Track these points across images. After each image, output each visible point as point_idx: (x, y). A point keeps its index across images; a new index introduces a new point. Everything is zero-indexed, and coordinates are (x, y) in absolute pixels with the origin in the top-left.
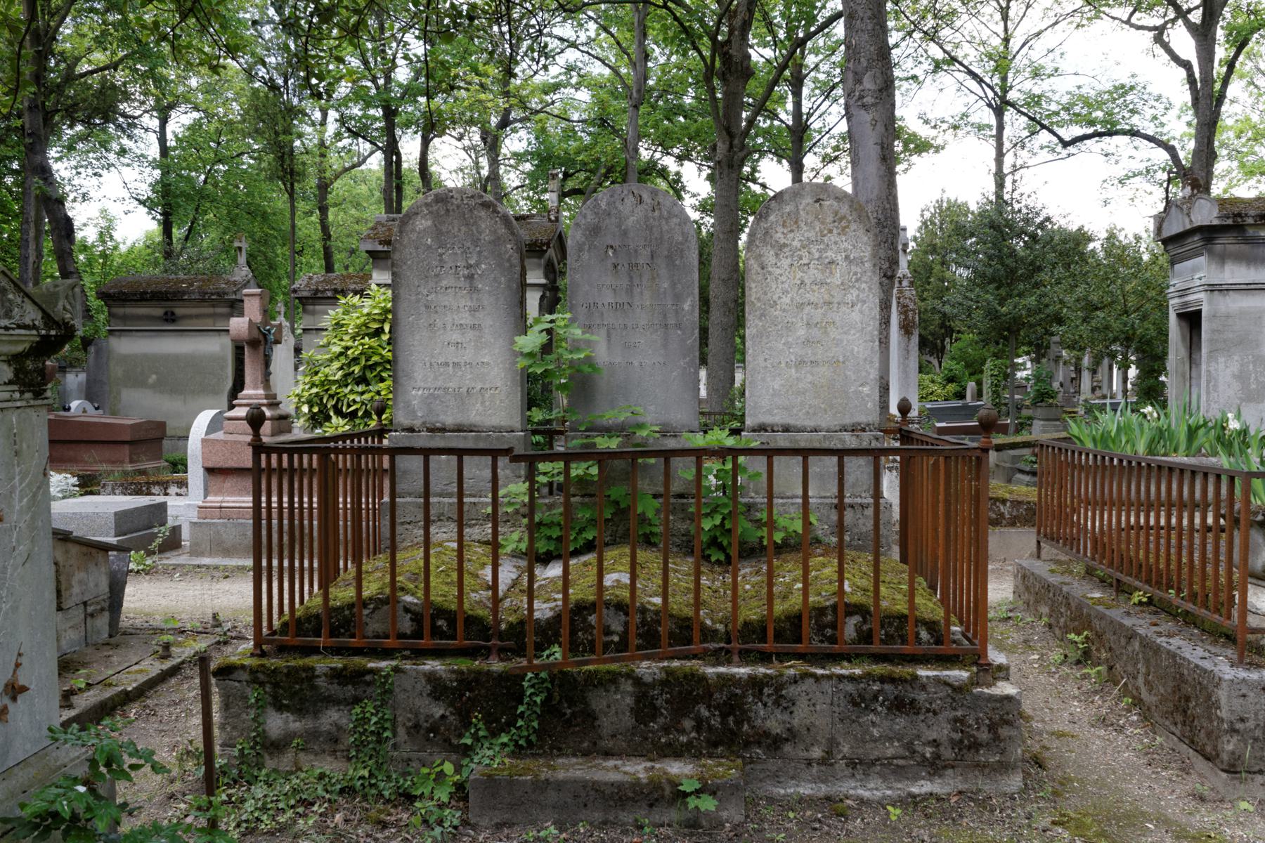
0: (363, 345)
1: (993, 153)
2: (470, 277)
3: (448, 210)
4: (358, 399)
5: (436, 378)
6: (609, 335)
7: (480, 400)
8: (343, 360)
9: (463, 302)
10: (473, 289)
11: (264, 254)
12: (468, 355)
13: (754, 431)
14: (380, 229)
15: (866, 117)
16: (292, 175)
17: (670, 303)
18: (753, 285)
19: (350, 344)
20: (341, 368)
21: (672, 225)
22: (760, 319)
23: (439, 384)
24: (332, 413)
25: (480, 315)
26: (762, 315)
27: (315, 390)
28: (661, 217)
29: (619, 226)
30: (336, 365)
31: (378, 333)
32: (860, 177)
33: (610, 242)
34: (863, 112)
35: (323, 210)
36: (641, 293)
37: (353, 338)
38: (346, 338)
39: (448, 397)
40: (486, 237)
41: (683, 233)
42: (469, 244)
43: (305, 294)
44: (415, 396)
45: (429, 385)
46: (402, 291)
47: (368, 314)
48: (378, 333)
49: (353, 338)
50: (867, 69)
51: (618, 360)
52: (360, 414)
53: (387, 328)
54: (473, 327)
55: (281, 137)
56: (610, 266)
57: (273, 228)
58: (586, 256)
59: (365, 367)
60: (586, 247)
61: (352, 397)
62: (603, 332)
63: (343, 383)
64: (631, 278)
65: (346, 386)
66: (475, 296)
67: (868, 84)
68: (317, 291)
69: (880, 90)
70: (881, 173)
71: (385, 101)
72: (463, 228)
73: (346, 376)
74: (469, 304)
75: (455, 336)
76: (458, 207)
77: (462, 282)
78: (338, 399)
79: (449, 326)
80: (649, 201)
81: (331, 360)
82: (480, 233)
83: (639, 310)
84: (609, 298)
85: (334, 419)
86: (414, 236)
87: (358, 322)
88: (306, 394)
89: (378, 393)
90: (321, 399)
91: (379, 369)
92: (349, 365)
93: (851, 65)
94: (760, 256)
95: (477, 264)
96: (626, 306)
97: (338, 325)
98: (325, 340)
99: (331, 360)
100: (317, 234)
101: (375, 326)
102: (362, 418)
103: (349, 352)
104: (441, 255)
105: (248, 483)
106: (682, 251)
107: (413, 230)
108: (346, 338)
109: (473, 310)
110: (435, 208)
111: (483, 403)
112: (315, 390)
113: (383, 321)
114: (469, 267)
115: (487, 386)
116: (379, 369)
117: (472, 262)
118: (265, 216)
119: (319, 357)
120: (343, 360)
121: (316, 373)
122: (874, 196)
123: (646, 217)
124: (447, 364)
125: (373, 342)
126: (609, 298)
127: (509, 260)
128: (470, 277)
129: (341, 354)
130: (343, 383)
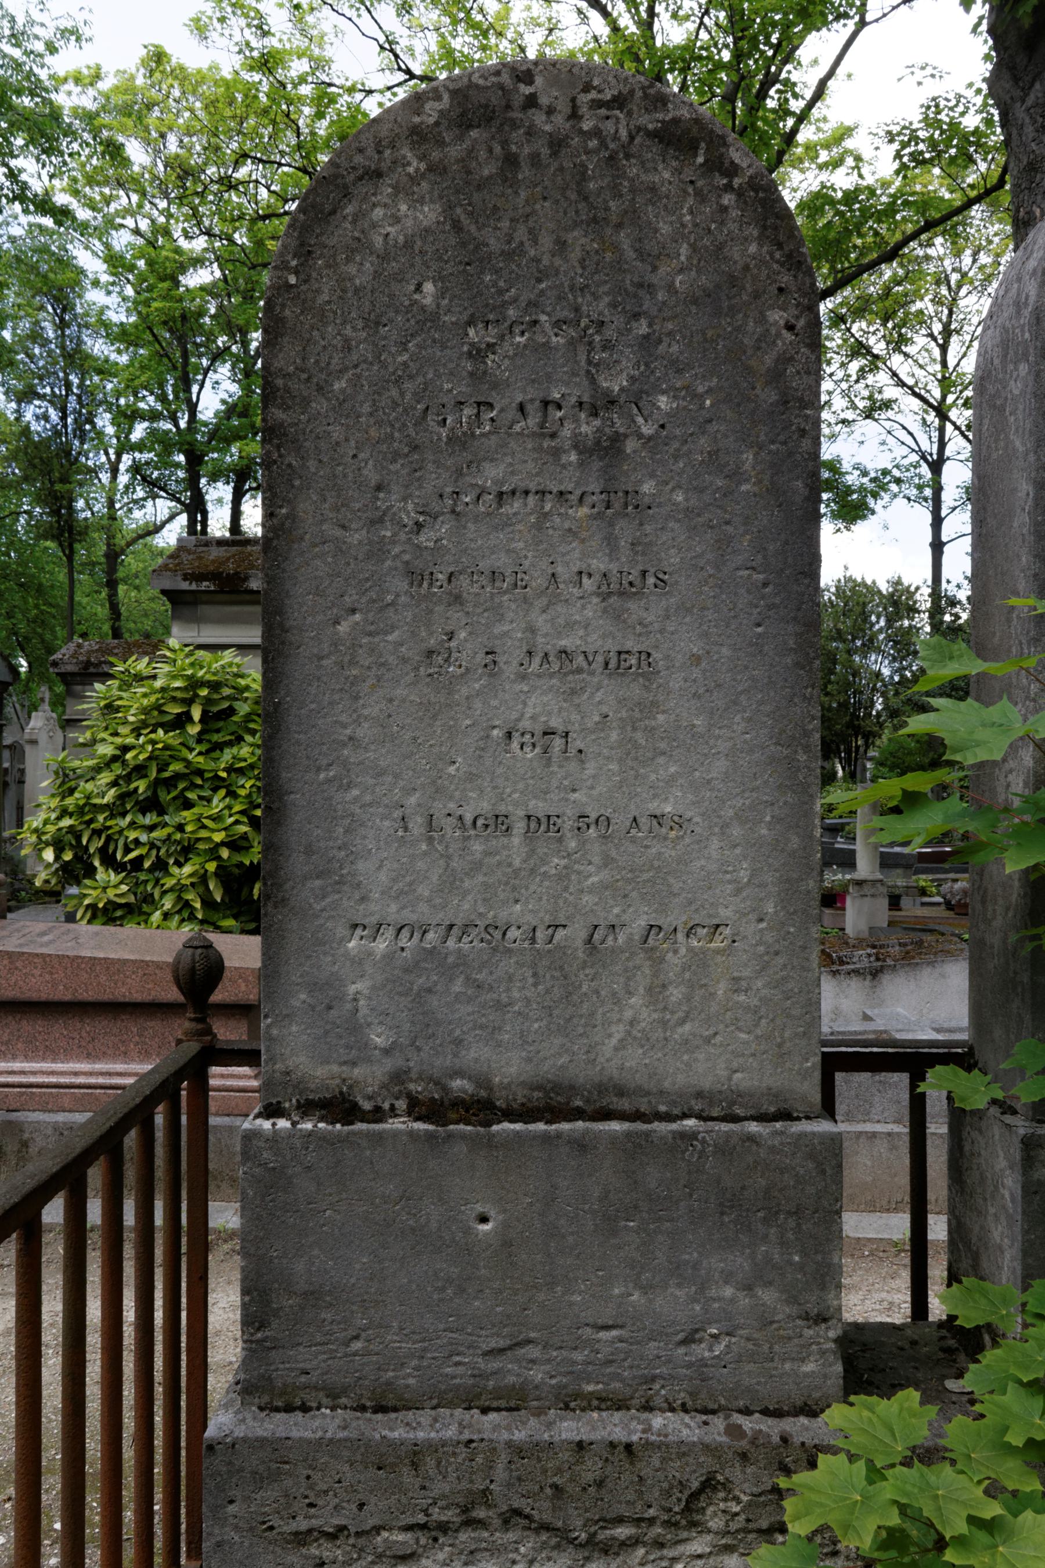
0: (153, 742)
1: (928, 518)
2: (607, 449)
3: (511, 161)
4: (144, 838)
5: (450, 883)
7: (642, 981)
8: (118, 769)
9: (572, 558)
10: (618, 502)
11: (41, 636)
12: (592, 785)
14: (185, 557)
16: (70, 532)
19: (130, 740)
20: (115, 784)
23: (462, 909)
24: (97, 863)
25: (647, 610)
27: (66, 822)
30: (105, 778)
31: (181, 721)
35: (112, 584)
37: (137, 732)
38: (124, 730)
39: (506, 965)
40: (678, 275)
42: (602, 307)
43: (70, 668)
44: (358, 962)
45: (422, 912)
46: (305, 507)
47: (163, 690)
48: (181, 721)
49: (137, 732)
52: (147, 864)
53: (196, 713)
54: (617, 664)
55: (58, 487)
57: (51, 605)
59: (157, 783)
61: (132, 835)
63: (116, 810)
65: (123, 815)
66: (625, 531)
68: (88, 664)
71: (189, 443)
72: (579, 240)
73: (122, 797)
74: (598, 564)
75: (540, 704)
76: (557, 144)
77: (569, 473)
78: (109, 838)
79: (509, 663)
81: (98, 770)
82: (652, 259)
85: (101, 875)
86: (361, 272)
87: (145, 702)
88: (51, 829)
89: (180, 828)
90: (78, 837)
91: (181, 786)
92: (128, 778)
95: (638, 397)
97: (110, 708)
98: (88, 735)
99: (98, 770)
100: (102, 611)
101: (176, 710)
102: (151, 870)
103: (129, 756)
104: (478, 354)
105: (259, 652)
107: (360, 245)
108: (124, 730)
109: (617, 592)
110: (455, 151)
111: (656, 992)
112: (66, 822)
113: (189, 702)
114: (600, 404)
115: (675, 918)
116: (181, 786)
117: (615, 384)
118: (40, 590)
119: (76, 763)
120: (118, 769)
121: (71, 791)
124: (500, 822)
125: (172, 738)
128: (607, 449)
129: (114, 759)
130: (116, 810)
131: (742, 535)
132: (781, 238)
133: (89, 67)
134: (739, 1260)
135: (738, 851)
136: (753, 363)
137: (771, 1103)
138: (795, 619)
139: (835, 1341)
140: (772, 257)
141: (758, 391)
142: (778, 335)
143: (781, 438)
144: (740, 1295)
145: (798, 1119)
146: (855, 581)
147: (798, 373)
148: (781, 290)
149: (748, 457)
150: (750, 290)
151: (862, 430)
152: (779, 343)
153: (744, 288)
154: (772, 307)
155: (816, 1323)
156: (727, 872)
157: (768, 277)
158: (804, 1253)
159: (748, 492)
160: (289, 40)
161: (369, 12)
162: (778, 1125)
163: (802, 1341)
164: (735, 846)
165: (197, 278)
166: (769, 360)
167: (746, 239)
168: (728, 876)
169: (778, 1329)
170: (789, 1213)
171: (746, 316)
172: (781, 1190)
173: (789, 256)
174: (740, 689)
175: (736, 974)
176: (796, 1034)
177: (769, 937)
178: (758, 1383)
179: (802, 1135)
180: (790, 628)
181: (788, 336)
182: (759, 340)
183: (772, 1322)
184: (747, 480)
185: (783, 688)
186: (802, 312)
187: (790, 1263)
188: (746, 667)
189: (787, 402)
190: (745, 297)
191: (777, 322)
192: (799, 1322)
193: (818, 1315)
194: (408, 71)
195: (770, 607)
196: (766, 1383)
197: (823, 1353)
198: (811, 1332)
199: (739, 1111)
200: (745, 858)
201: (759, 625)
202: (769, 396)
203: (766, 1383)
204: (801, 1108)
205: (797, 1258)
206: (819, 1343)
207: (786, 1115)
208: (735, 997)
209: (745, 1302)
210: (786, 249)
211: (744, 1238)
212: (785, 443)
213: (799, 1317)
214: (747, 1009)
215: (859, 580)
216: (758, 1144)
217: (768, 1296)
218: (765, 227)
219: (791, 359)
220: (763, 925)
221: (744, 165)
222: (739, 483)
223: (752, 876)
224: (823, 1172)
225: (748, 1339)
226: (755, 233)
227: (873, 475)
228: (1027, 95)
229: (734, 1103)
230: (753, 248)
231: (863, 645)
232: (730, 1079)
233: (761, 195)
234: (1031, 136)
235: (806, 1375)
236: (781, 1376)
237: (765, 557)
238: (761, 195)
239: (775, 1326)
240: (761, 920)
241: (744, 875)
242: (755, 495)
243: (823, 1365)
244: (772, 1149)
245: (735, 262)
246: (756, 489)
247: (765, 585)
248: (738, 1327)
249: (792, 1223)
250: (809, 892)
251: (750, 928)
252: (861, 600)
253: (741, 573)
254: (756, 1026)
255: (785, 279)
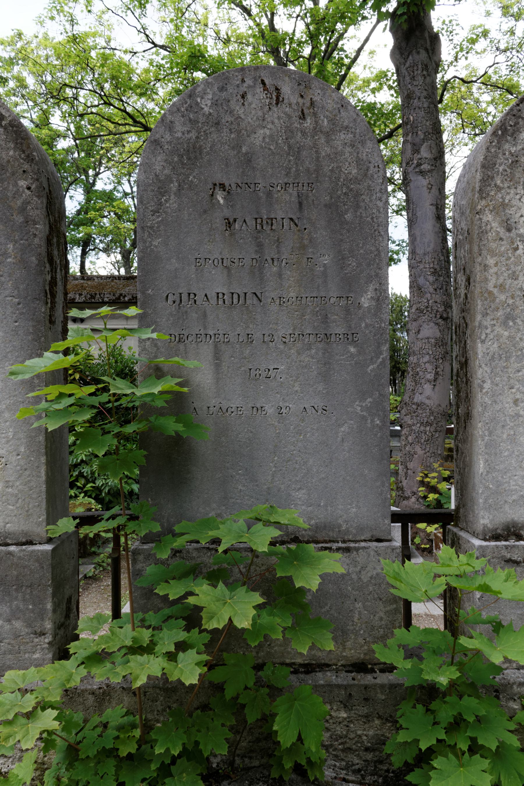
6: (217, 355)
13: (496, 537)
15: (422, 182)
17: (334, 292)
18: (491, 261)
21: (338, 144)
22: (505, 324)
26: (509, 317)
28: (317, 129)
29: (237, 147)
32: (418, 233)
33: (219, 177)
34: (420, 178)
36: (280, 275)
41: (359, 162)
50: (423, 140)
51: (235, 402)
56: (219, 224)
58: (172, 203)
60: (174, 186)
62: (207, 350)
64: (260, 245)
67: (425, 153)
69: (435, 159)
70: (437, 229)
80: (294, 99)
83: (274, 308)
84: (217, 283)
93: (409, 138)
94: (504, 205)
96: (251, 300)
106: (358, 195)
122: (430, 249)
123: (290, 131)
126: (217, 283)
127: (23, 210)
131: (8, 281)
132: (24, 148)
133: (8, 37)
134: (5, 608)
135: (8, 424)
136: (12, 204)
137: (23, 537)
138: (32, 319)
139: (49, 643)
140: (20, 157)
141: (14, 217)
142: (23, 191)
143: (25, 238)
144: (5, 624)
145: (36, 544)
146: (397, 295)
147: (32, 208)
148: (24, 171)
149: (11, 246)
150: (10, 171)
151: (396, 221)
152: (24, 195)
153: (7, 170)
154: (20, 179)
155: (40, 636)
156: (3, 433)
157: (19, 165)
158: (34, 604)
159: (11, 262)
160: (94, 27)
161: (133, 14)
162: (24, 547)
163: (33, 644)
164: (6, 422)
165: (62, 144)
166: (19, 203)
167: (8, 149)
168: (3, 435)
169: (22, 639)
170: (27, 586)
171: (9, 183)
172: (23, 576)
173: (28, 156)
174: (8, 350)
175: (7, 479)
176: (35, 506)
177: (22, 463)
178: (13, 664)
179: (33, 551)
180: (30, 323)
181: (28, 192)
182: (14, 194)
183: (20, 636)
184: (10, 257)
185: (27, 350)
186: (34, 181)
187: (28, 609)
188: (10, 341)
189: (27, 222)
190: (8, 175)
191: (22, 186)
192: (32, 636)
193: (41, 632)
194: (153, 43)
195: (22, 313)
196: (17, 664)
197: (43, 649)
198: (37, 640)
199: (9, 541)
200: (11, 427)
201: (16, 322)
202: (20, 219)
203: (17, 664)
204: (36, 539)
205: (31, 607)
206: (41, 645)
207: (30, 543)
208: (7, 490)
209: (7, 627)
210: (26, 153)
211: (7, 598)
212: (27, 240)
213: (32, 633)
214: (12, 495)
215: (399, 295)
216: (13, 556)
217: (18, 624)
218: (17, 143)
219: (29, 202)
220: (19, 457)
221: (7, 115)
222: (6, 258)
223: (14, 435)
224: (43, 567)
225: (9, 644)
226: (12, 146)
227: (397, 243)
228: (406, 61)
229: (7, 538)
230: (11, 153)
231: (401, 327)
232: (5, 527)
233: (15, 129)
234: (409, 81)
235: (35, 659)
236: (24, 660)
237: (18, 291)
238: (15, 129)
239: (21, 637)
240: (18, 455)
241: (11, 435)
242: (14, 263)
243: (43, 654)
244: (20, 558)
245: (4, 159)
246: (14, 261)
247: (19, 304)
248: (4, 639)
249: (28, 591)
250: (40, 442)
251: (13, 459)
252: (400, 304)
253: (8, 298)
254: (17, 502)
255: (26, 167)
